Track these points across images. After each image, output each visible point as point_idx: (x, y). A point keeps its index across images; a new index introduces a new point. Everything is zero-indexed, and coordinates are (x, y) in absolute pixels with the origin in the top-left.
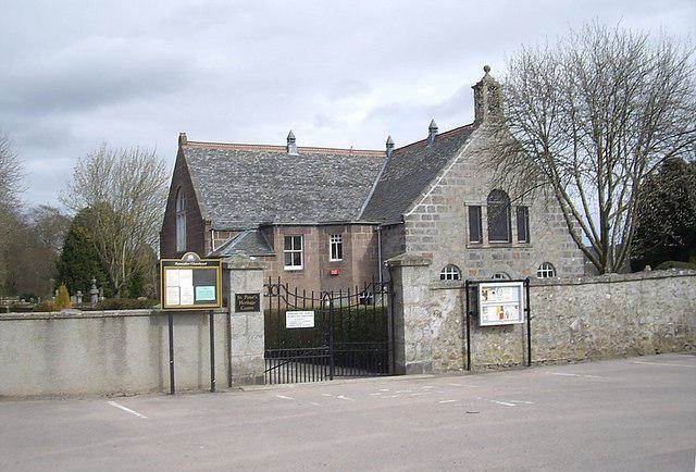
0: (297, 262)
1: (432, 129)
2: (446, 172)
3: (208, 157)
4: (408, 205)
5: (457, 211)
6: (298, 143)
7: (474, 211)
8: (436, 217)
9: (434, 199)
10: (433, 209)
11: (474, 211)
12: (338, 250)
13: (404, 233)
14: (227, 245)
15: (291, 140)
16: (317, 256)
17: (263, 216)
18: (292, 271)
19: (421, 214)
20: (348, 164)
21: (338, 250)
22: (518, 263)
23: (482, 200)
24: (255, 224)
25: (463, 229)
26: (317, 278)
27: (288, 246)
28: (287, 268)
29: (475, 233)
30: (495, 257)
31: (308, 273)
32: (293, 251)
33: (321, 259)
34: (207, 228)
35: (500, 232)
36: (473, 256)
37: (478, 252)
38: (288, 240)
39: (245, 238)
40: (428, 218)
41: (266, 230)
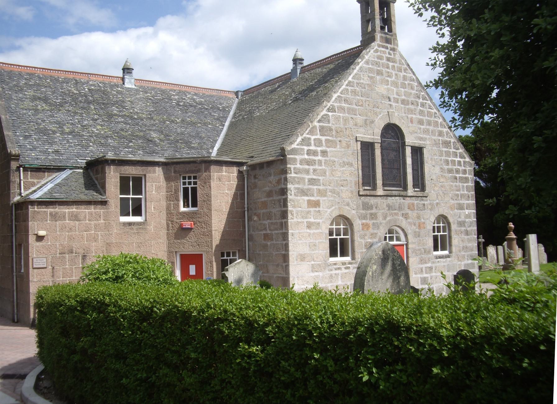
0: (137, 211)
1: (296, 61)
2: (335, 96)
3: (24, 82)
4: (289, 135)
5: (348, 146)
6: (136, 74)
7: (367, 148)
8: (324, 153)
9: (322, 129)
10: (318, 143)
11: (367, 148)
12: (191, 197)
13: (285, 172)
14: (39, 188)
15: (127, 70)
16: (164, 203)
17: (94, 151)
18: (130, 224)
19: (306, 148)
20: (202, 105)
21: (191, 197)
22: (413, 214)
23: (374, 135)
24: (82, 162)
25: (353, 171)
26: (163, 233)
27: (124, 189)
28: (436, 253)
29: (368, 179)
30: (389, 207)
31: (151, 228)
32: (131, 196)
33: (168, 208)
34: (14, 165)
35: (395, 179)
36: (366, 207)
37: (372, 201)
38: (124, 183)
39: (66, 179)
40: (315, 153)
41: (94, 171)
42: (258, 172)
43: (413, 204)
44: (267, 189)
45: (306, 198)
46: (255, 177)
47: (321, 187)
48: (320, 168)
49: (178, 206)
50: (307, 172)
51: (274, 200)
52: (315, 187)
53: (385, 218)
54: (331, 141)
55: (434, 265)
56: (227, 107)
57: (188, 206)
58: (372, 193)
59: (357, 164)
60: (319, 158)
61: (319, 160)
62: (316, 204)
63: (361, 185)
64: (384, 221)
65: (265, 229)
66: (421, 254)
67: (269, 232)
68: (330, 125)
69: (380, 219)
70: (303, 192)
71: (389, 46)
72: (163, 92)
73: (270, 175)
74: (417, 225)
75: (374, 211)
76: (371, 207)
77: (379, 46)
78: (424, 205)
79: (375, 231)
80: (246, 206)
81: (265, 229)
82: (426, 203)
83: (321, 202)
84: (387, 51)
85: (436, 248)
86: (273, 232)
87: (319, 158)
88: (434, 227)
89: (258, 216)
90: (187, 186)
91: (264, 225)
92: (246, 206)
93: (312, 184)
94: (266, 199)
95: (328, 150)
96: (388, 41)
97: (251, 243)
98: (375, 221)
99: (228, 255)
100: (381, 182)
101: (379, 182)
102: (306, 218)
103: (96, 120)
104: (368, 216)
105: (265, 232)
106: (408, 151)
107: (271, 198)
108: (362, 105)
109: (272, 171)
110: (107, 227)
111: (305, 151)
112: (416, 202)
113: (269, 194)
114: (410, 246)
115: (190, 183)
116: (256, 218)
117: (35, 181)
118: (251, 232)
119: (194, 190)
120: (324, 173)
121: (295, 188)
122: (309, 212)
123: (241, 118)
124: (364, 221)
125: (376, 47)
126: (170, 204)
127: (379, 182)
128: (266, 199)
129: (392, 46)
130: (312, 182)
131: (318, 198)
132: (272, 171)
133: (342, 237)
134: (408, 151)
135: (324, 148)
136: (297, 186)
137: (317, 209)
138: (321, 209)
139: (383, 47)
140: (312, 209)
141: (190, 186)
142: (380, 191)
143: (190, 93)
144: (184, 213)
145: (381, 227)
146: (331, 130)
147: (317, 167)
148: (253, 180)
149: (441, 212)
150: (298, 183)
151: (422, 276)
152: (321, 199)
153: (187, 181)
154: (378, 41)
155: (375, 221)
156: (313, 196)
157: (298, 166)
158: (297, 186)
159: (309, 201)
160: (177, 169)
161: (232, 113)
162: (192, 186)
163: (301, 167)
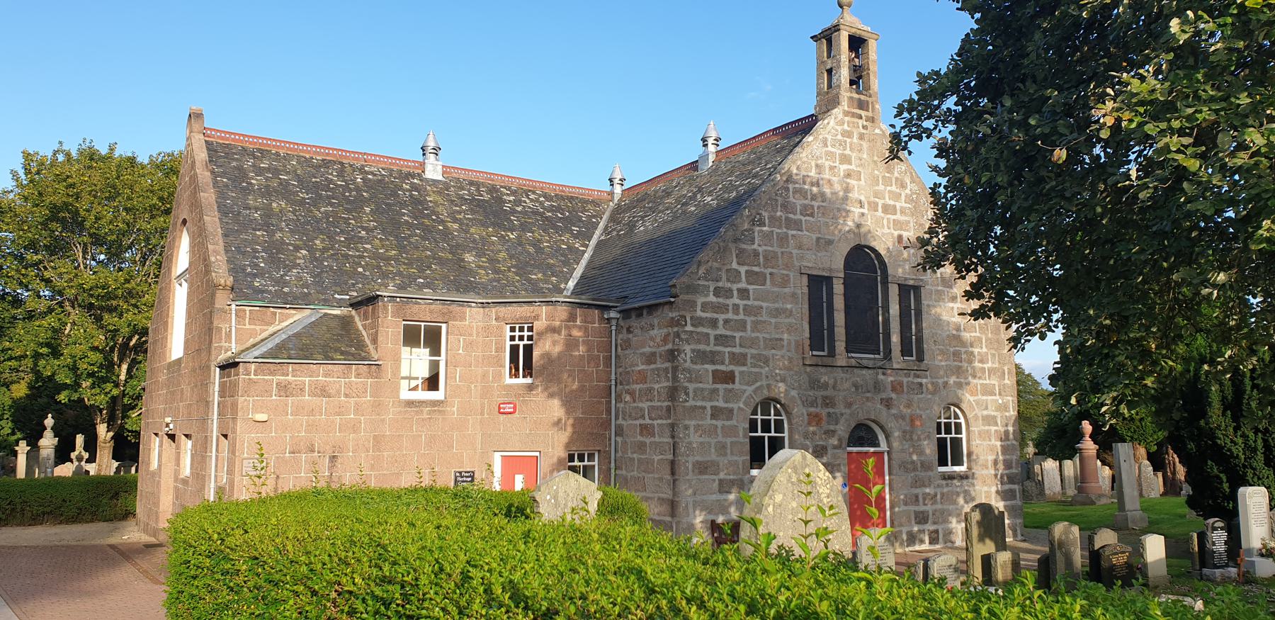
7: (818, 284)
11: (818, 284)
23: (835, 263)
25: (793, 324)
29: (819, 336)
42: (634, 322)
43: (901, 384)
44: (647, 350)
45: (710, 367)
46: (629, 331)
47: (737, 350)
48: (736, 317)
49: (499, 376)
50: (713, 323)
51: (658, 369)
52: (729, 349)
53: (849, 405)
54: (757, 273)
55: (939, 491)
56: (594, 217)
57: (516, 376)
58: (829, 361)
59: (801, 310)
60: (736, 300)
61: (734, 305)
62: (729, 378)
63: (807, 348)
64: (848, 411)
65: (643, 417)
66: (915, 469)
67: (648, 421)
68: (755, 246)
69: (840, 408)
70: (701, 357)
71: (863, 113)
72: (493, 190)
73: (652, 327)
74: (908, 419)
75: (829, 392)
76: (825, 386)
77: (846, 114)
78: (921, 384)
79: (832, 427)
80: (613, 377)
81: (643, 417)
82: (924, 381)
83: (737, 374)
84: (860, 122)
85: (943, 462)
86: (655, 422)
87: (736, 300)
88: (939, 424)
89: (632, 393)
90: (517, 342)
91: (642, 409)
92: (613, 377)
93: (722, 345)
94: (643, 367)
95: (751, 287)
96: (862, 105)
97: (619, 439)
98: (831, 410)
99: (581, 459)
100: (844, 344)
101: (840, 346)
102: (711, 400)
103: (372, 230)
104: (820, 401)
105: (642, 422)
106: (894, 291)
107: (653, 366)
108: (812, 215)
109: (656, 321)
110: (377, 406)
111: (712, 289)
112: (905, 380)
113: (650, 358)
114: (894, 456)
115: (521, 338)
116: (628, 398)
117: (258, 328)
118: (620, 421)
119: (529, 350)
120: (742, 326)
121: (693, 351)
122: (715, 391)
123: (615, 233)
124: (812, 409)
125: (841, 116)
126: (488, 372)
127: (840, 346)
128: (643, 367)
129: (870, 114)
130: (721, 340)
131: (731, 368)
132: (656, 321)
133: (773, 434)
134: (894, 291)
135: (743, 285)
136: (693, 347)
137: (730, 386)
138: (737, 386)
139: (853, 115)
140: (720, 386)
141: (521, 343)
142: (841, 359)
143: (534, 192)
144: (511, 386)
145: (842, 421)
146: (756, 254)
147: (730, 316)
148: (624, 335)
149: (862, 417)
150: (699, 342)
151: (917, 508)
152: (737, 370)
153: (517, 334)
154: (845, 105)
155: (831, 410)
156: (723, 363)
157: (699, 313)
158: (693, 347)
159: (714, 372)
160: (501, 315)
161: (601, 225)
162: (526, 342)
163: (704, 315)
